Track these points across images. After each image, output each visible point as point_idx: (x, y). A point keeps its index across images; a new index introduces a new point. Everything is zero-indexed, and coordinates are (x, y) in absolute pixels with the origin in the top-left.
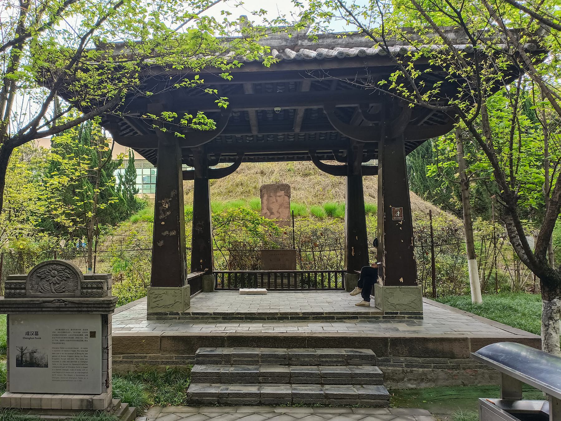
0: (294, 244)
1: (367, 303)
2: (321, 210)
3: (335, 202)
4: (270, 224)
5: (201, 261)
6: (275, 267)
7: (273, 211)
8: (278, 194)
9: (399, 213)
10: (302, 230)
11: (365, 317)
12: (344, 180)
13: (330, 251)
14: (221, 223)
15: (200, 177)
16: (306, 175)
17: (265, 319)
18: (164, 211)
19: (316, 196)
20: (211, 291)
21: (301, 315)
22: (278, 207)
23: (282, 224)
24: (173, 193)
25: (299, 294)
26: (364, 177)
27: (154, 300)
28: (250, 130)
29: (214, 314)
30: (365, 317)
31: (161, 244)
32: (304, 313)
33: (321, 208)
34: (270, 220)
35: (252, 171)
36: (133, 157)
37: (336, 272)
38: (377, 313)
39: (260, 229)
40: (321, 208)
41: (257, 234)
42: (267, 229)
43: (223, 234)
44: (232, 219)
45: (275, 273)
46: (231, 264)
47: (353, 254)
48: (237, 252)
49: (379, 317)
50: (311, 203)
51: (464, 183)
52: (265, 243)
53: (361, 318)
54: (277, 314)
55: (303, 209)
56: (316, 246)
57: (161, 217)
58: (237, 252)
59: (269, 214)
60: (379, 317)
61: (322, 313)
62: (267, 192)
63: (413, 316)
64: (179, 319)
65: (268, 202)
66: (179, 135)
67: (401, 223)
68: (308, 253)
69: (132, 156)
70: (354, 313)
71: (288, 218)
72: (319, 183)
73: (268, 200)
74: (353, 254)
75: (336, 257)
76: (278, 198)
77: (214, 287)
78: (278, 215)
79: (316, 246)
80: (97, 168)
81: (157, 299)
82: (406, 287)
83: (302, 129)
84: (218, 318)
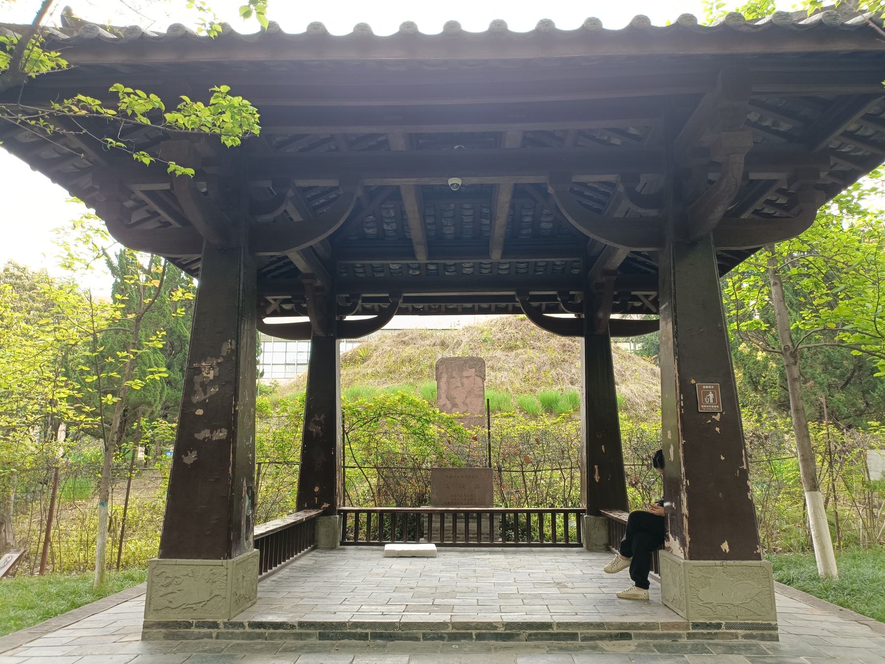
0: (490, 458)
1: (642, 593)
2: (533, 401)
3: (556, 389)
4: (449, 423)
5: (317, 489)
6: (452, 507)
8: (465, 374)
9: (711, 395)
10: (504, 432)
11: (646, 636)
12: (579, 344)
13: (552, 470)
14: (364, 419)
15: (320, 333)
16: (511, 349)
17: (416, 639)
18: (204, 386)
19: (526, 380)
20: (333, 548)
21: (501, 630)
22: (464, 396)
23: (470, 422)
24: (227, 347)
25: (498, 556)
26: (612, 339)
27: (164, 591)
28: (412, 255)
29: (302, 625)
30: (646, 636)
31: (191, 458)
32: (508, 625)
33: (534, 399)
34: (448, 416)
35: (428, 342)
37: (566, 513)
38: (674, 626)
39: (433, 430)
40: (534, 399)
42: (443, 431)
43: (367, 439)
44: (383, 412)
45: (455, 513)
46: (380, 493)
47: (597, 478)
48: (389, 470)
49: (680, 636)
50: (518, 391)
51: (788, 353)
52: (441, 455)
53: (638, 636)
54: (444, 625)
55: (506, 399)
56: (528, 461)
57: (196, 399)
58: (389, 470)
59: (449, 406)
60: (680, 636)
61: (548, 625)
62: (447, 369)
63: (755, 632)
64: (217, 637)
65: (448, 387)
66: (181, 170)
67: (717, 418)
68: (514, 474)
70: (621, 625)
71: (481, 412)
72: (530, 360)
73: (448, 382)
74: (597, 478)
75: (567, 483)
76: (465, 380)
77: (340, 537)
79: (528, 461)
80: (134, 315)
81: (170, 589)
82: (737, 562)
83: (505, 254)
84: (308, 635)
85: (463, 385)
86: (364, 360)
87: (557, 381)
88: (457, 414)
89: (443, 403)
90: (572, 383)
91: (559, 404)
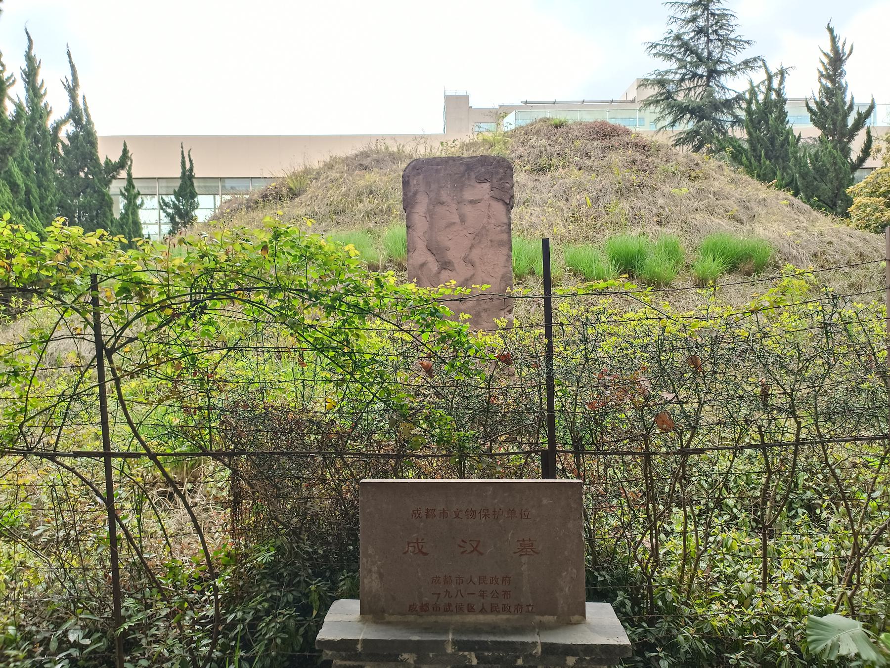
4: (430, 314)
7: (451, 255)
8: (468, 195)
16: (542, 170)
22: (467, 243)
34: (423, 292)
36: (191, 170)
39: (373, 339)
41: (358, 366)
59: (434, 267)
62: (428, 184)
65: (431, 226)
69: (188, 166)
72: (581, 188)
73: (430, 214)
76: (468, 210)
78: (464, 271)
85: (463, 219)
86: (293, 194)
87: (635, 218)
88: (449, 287)
89: (421, 260)
90: (659, 223)
91: (648, 261)
